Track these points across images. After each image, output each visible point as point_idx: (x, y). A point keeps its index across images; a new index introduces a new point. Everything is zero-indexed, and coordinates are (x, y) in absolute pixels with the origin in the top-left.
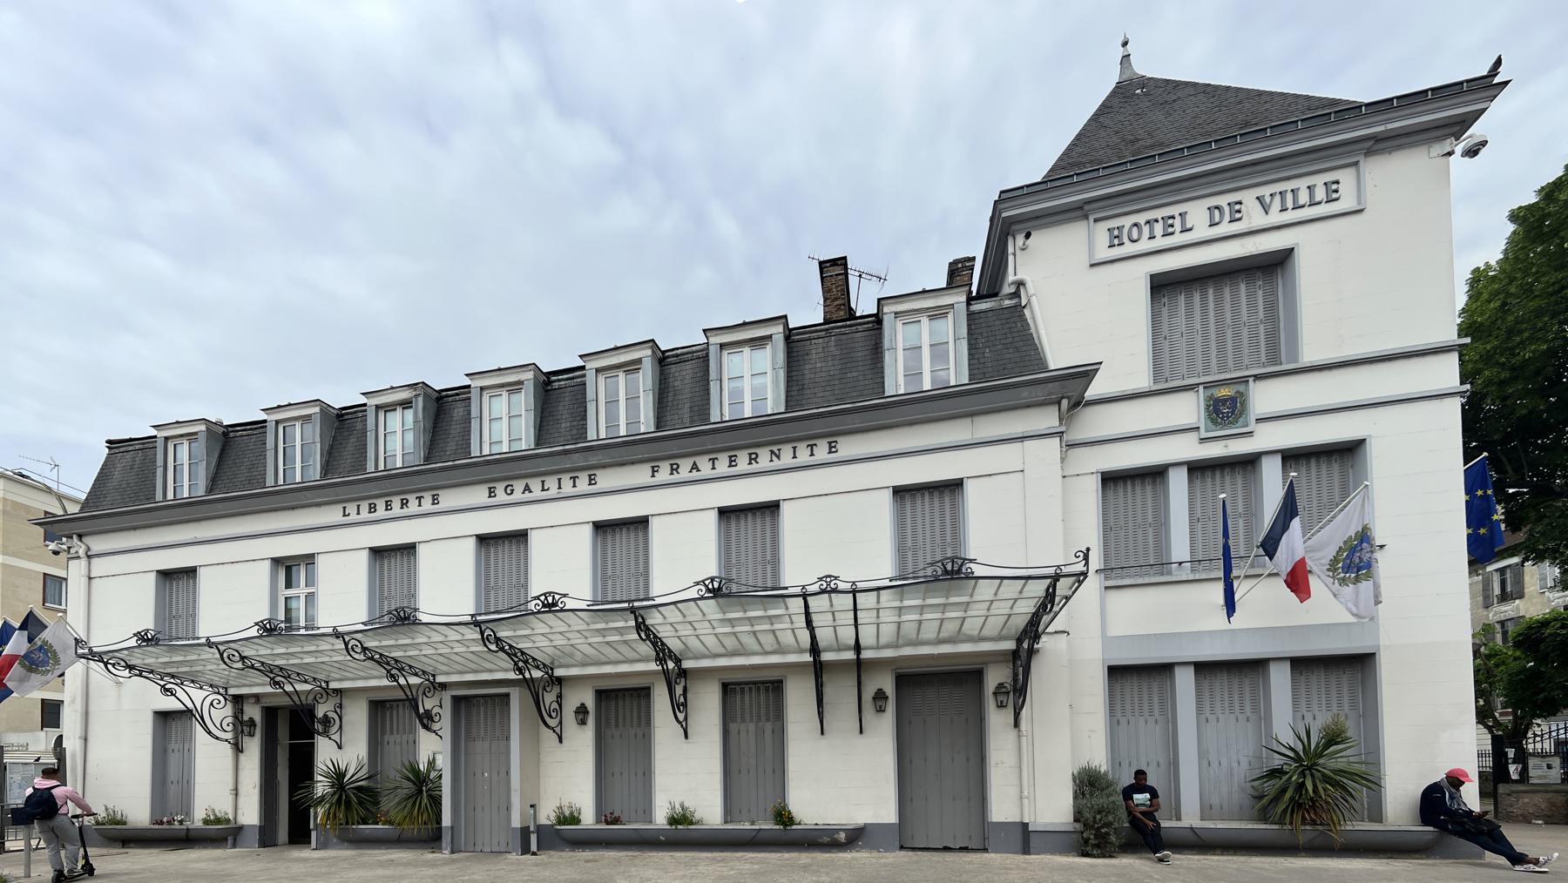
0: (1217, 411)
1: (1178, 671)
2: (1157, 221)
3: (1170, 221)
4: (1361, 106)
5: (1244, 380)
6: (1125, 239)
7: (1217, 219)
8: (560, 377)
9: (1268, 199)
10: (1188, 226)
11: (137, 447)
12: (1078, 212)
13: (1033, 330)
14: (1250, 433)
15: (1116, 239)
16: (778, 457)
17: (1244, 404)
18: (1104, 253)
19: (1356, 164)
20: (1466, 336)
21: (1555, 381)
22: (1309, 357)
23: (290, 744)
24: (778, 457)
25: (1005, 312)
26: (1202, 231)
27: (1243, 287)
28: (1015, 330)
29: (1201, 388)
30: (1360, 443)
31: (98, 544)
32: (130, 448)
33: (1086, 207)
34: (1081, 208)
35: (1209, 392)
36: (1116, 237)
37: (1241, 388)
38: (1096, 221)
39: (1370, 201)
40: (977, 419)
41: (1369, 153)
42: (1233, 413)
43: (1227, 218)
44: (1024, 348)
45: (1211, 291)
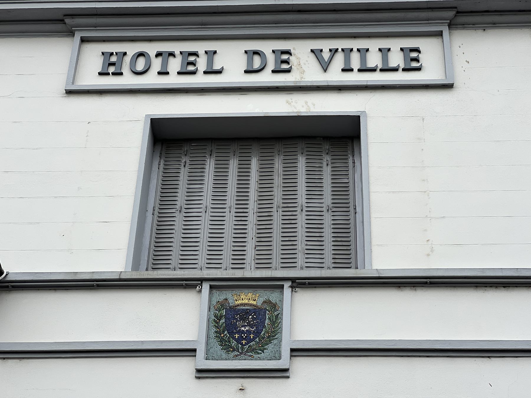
0: (231, 328)
2: (172, 54)
9: (326, 55)
10: (216, 67)
17: (276, 321)
19: (440, 34)
29: (206, 287)
33: (67, 21)
34: (62, 21)
35: (220, 296)
36: (113, 64)
37: (273, 297)
38: (83, 40)
42: (257, 333)
45: (254, 164)
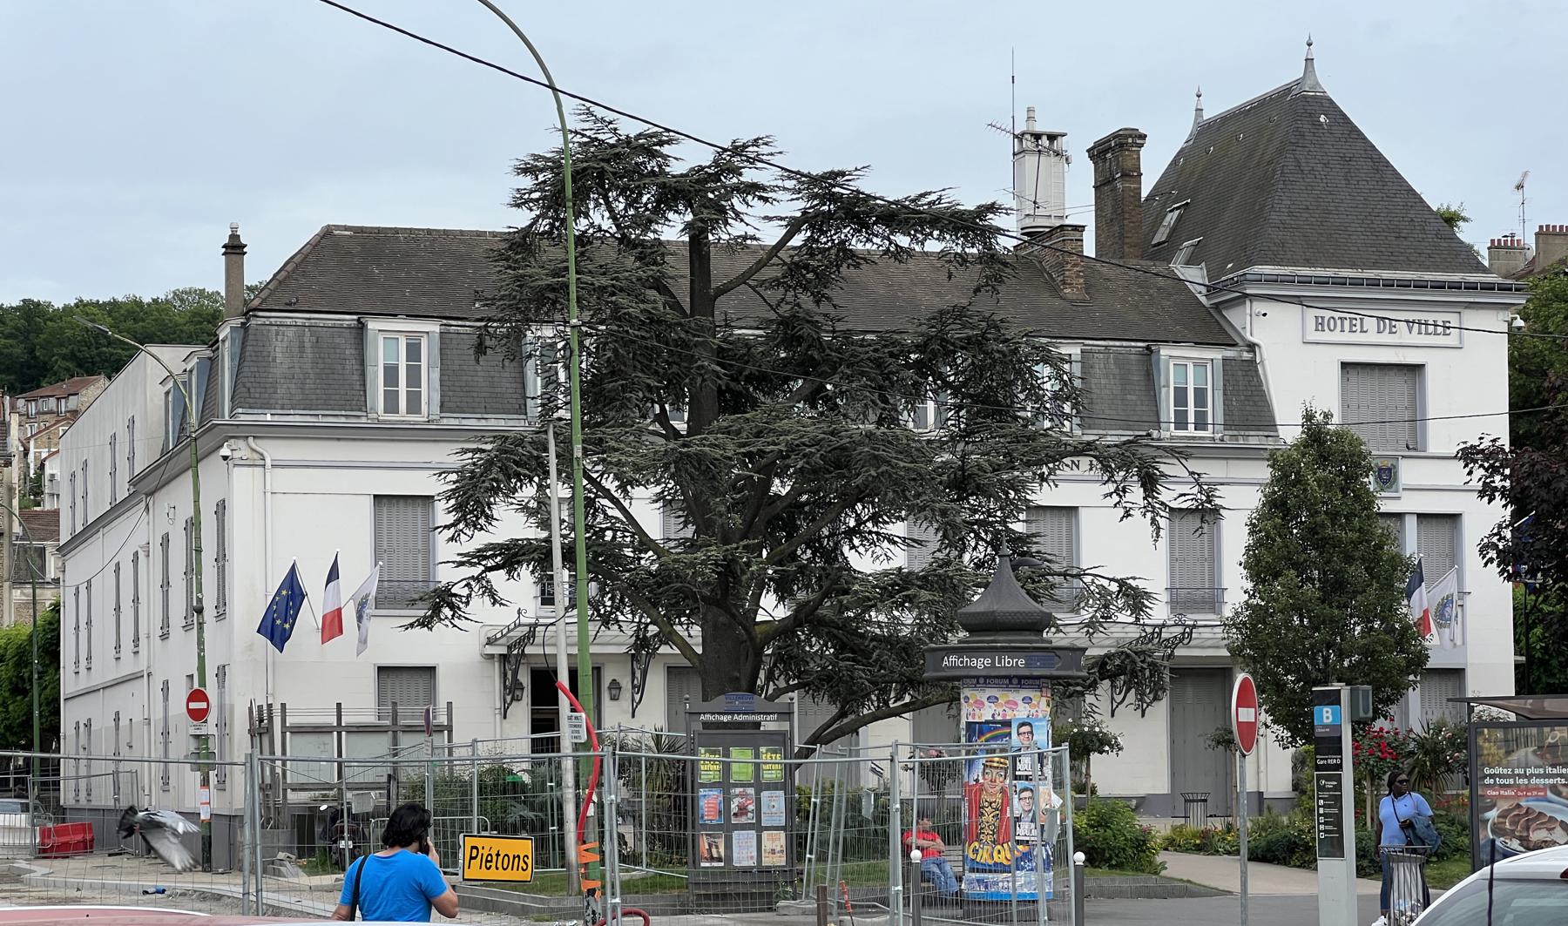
1: (1407, 518)
3: (1354, 322)
4: (215, 318)
5: (1396, 458)
6: (1326, 328)
7: (474, 855)
8: (1386, 274)
11: (300, 322)
12: (1298, 300)
13: (1265, 388)
14: (1399, 498)
15: (1320, 324)
16: (1078, 467)
17: (1396, 473)
18: (1314, 336)
20: (1521, 655)
21: (1561, 556)
22: (1432, 449)
23: (533, 740)
24: (1078, 467)
25: (1245, 364)
26: (1372, 337)
27: (419, 509)
28: (1253, 384)
30: (1459, 515)
31: (274, 450)
32: (288, 321)
39: (1466, 344)
40: (1230, 462)
41: (1466, 308)
43: (1387, 330)
44: (1260, 403)
